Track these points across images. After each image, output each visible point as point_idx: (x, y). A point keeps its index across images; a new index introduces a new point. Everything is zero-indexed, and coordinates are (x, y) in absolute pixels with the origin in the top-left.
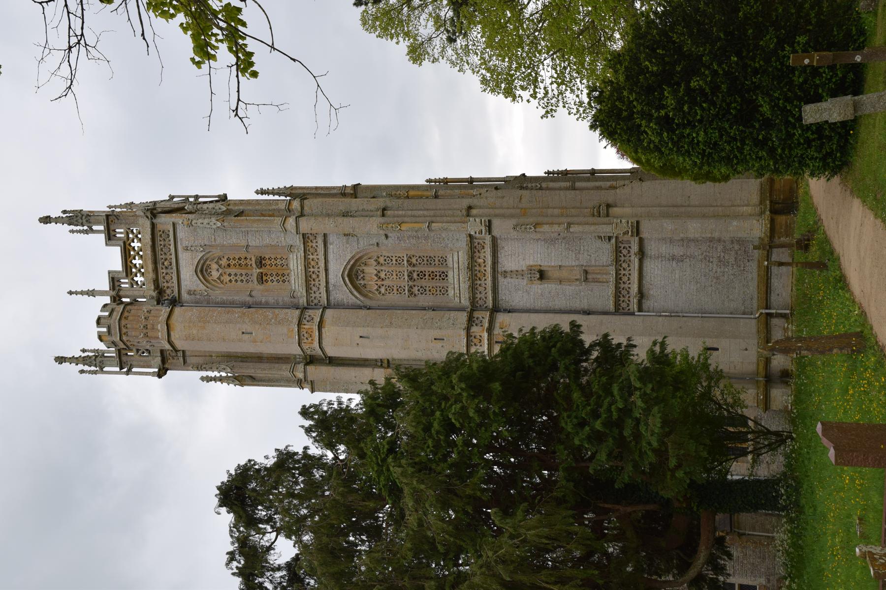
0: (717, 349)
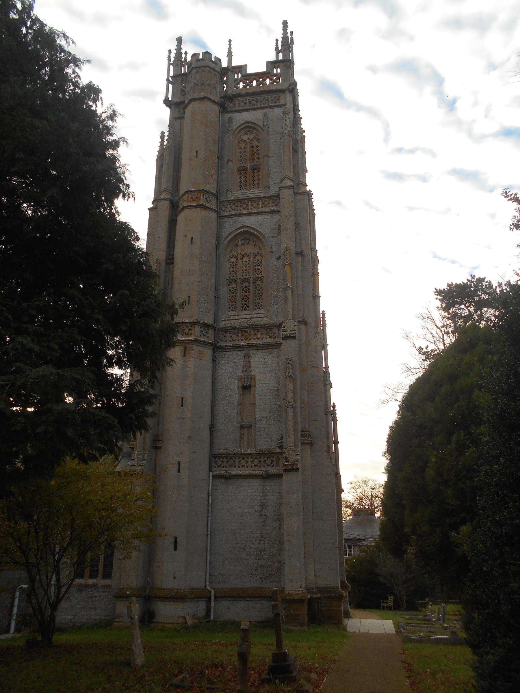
0: (175, 549)
